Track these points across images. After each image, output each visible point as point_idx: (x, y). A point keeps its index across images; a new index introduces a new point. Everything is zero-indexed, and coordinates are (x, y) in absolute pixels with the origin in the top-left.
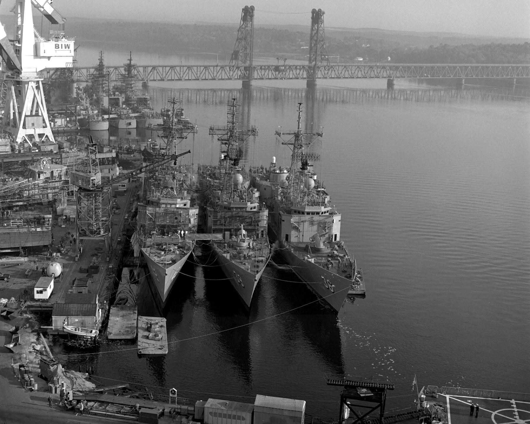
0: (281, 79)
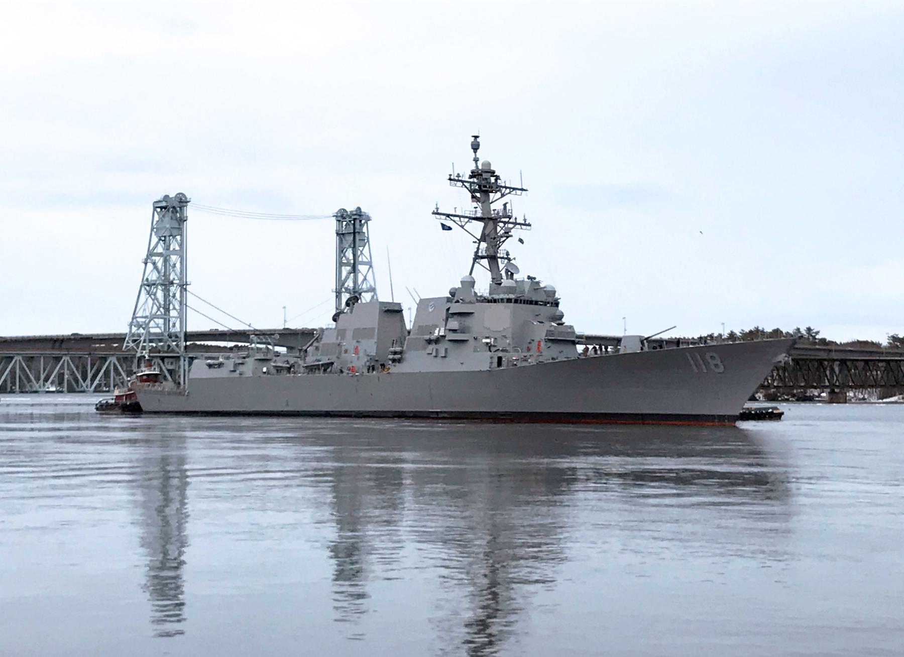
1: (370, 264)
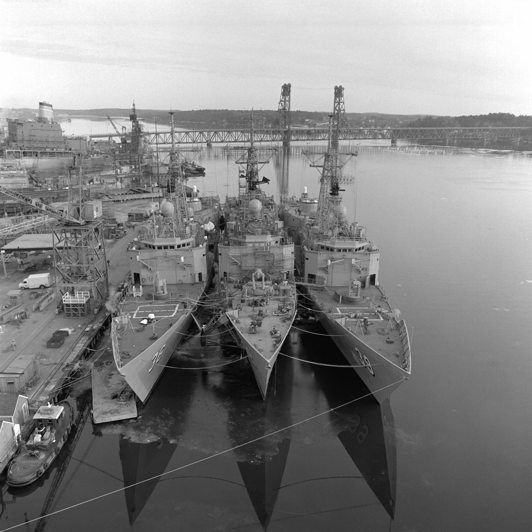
0: (312, 140)
1: (343, 102)
